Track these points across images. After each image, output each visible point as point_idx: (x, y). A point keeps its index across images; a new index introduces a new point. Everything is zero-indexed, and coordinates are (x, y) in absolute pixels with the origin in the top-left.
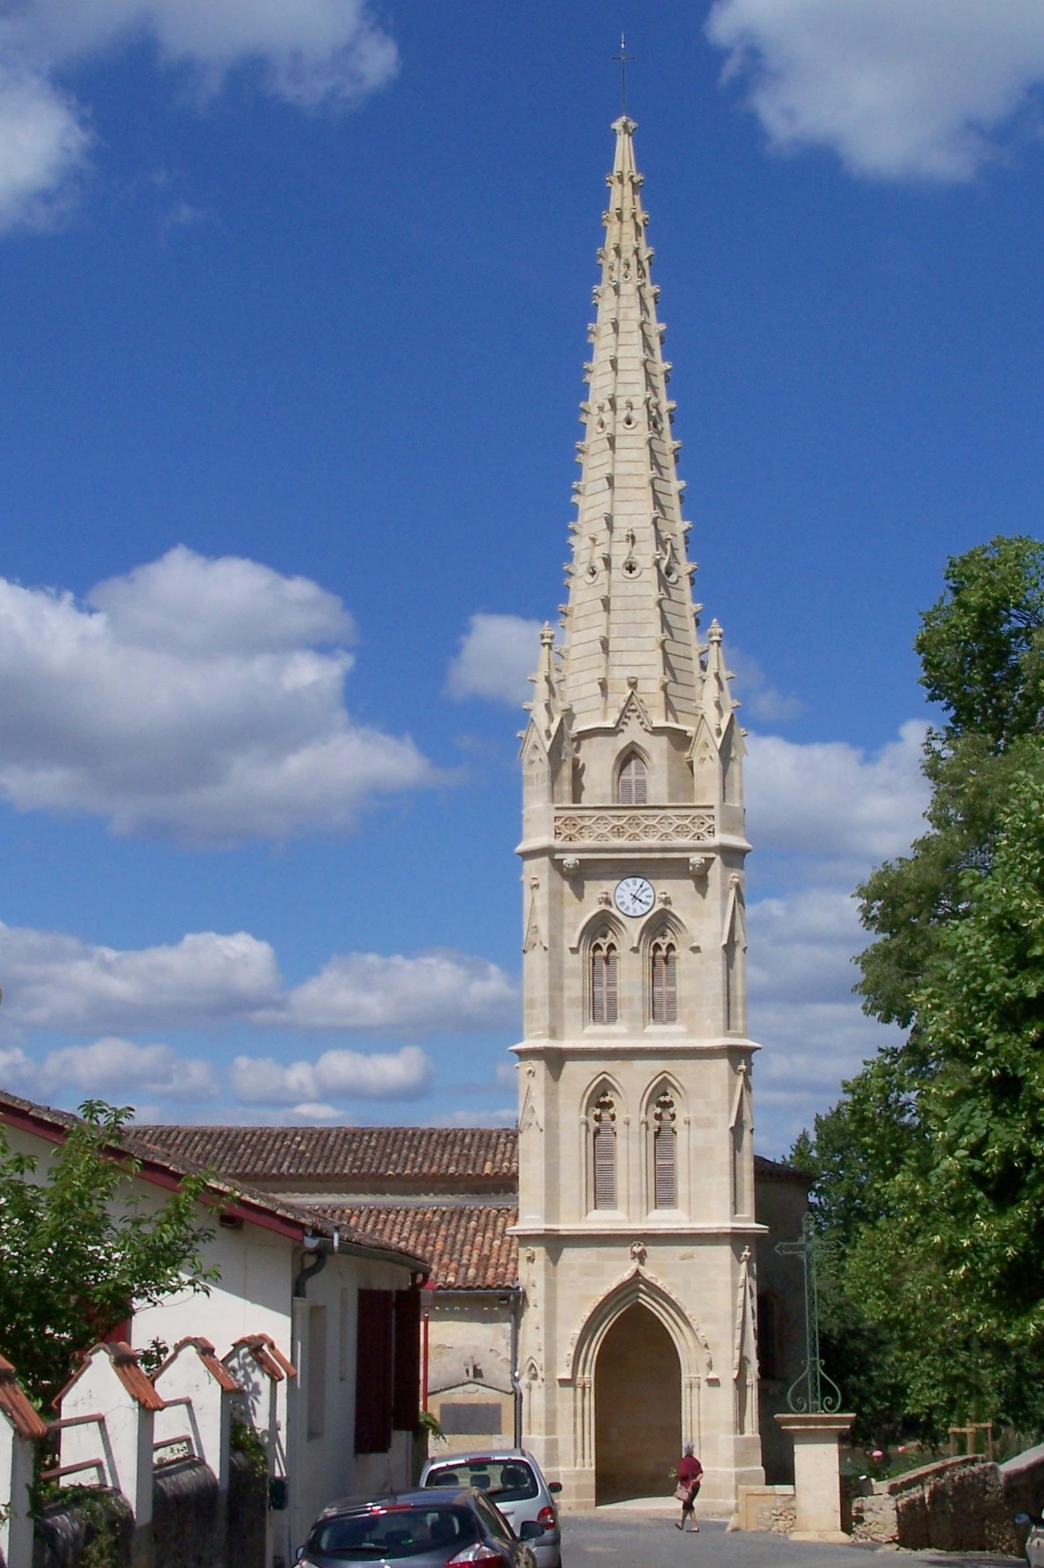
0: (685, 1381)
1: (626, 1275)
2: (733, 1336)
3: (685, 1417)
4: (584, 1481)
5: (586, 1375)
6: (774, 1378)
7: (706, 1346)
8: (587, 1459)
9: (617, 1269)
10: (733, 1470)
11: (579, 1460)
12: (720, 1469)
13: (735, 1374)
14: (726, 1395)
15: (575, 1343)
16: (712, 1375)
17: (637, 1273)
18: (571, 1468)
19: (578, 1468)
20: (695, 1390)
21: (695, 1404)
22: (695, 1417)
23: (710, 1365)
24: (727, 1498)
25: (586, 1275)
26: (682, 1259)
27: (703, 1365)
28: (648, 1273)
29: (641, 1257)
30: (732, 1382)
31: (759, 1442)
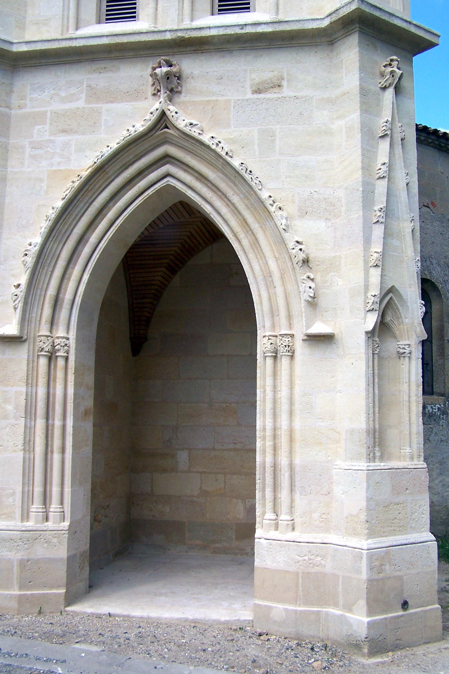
0: (263, 345)
1: (137, 119)
2: (367, 241)
3: (263, 421)
4: (40, 551)
5: (60, 332)
6: (432, 393)
7: (306, 262)
8: (54, 507)
9: (123, 110)
10: (365, 543)
11: (36, 507)
12: (333, 538)
13: (371, 321)
14: (351, 364)
15: (30, 260)
16: (319, 328)
17: (162, 120)
18: (16, 524)
19: (30, 524)
20: (284, 362)
21: (284, 393)
22: (284, 422)
23: (313, 303)
24: (349, 608)
25: (64, 131)
26: (258, 91)
27: (299, 306)
28: (181, 120)
29: (171, 85)
30: (363, 337)
31: (425, 478)
